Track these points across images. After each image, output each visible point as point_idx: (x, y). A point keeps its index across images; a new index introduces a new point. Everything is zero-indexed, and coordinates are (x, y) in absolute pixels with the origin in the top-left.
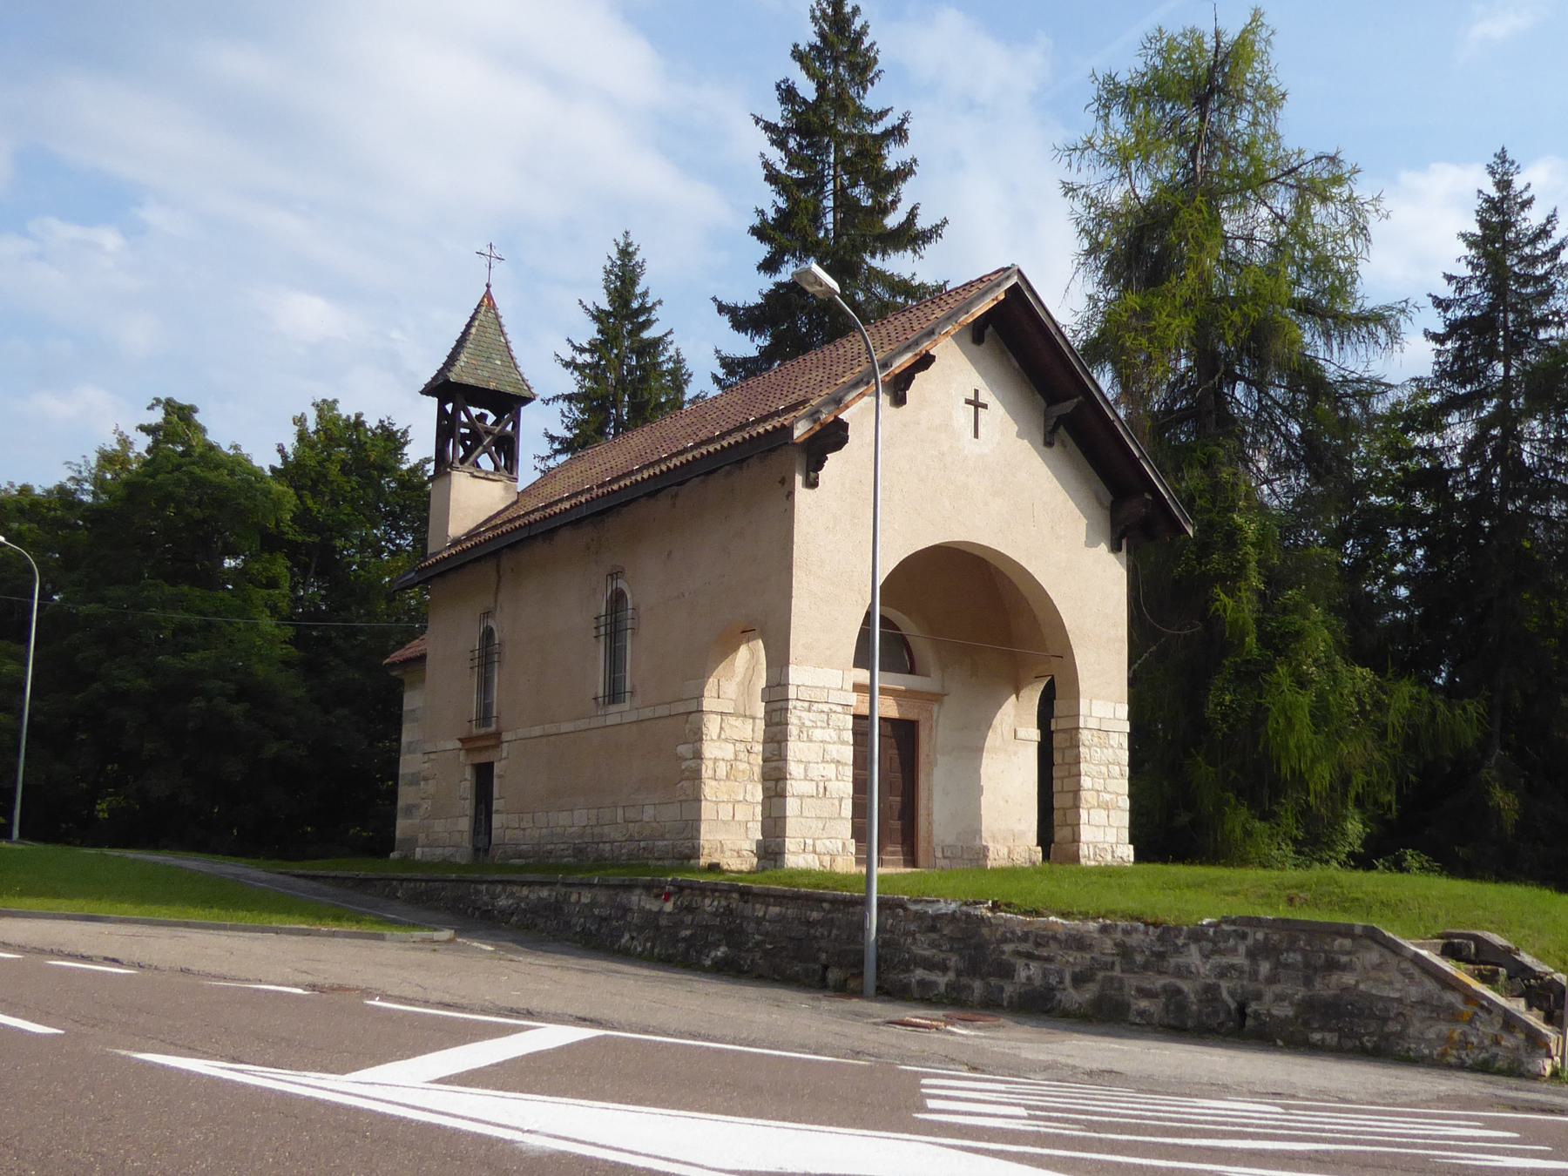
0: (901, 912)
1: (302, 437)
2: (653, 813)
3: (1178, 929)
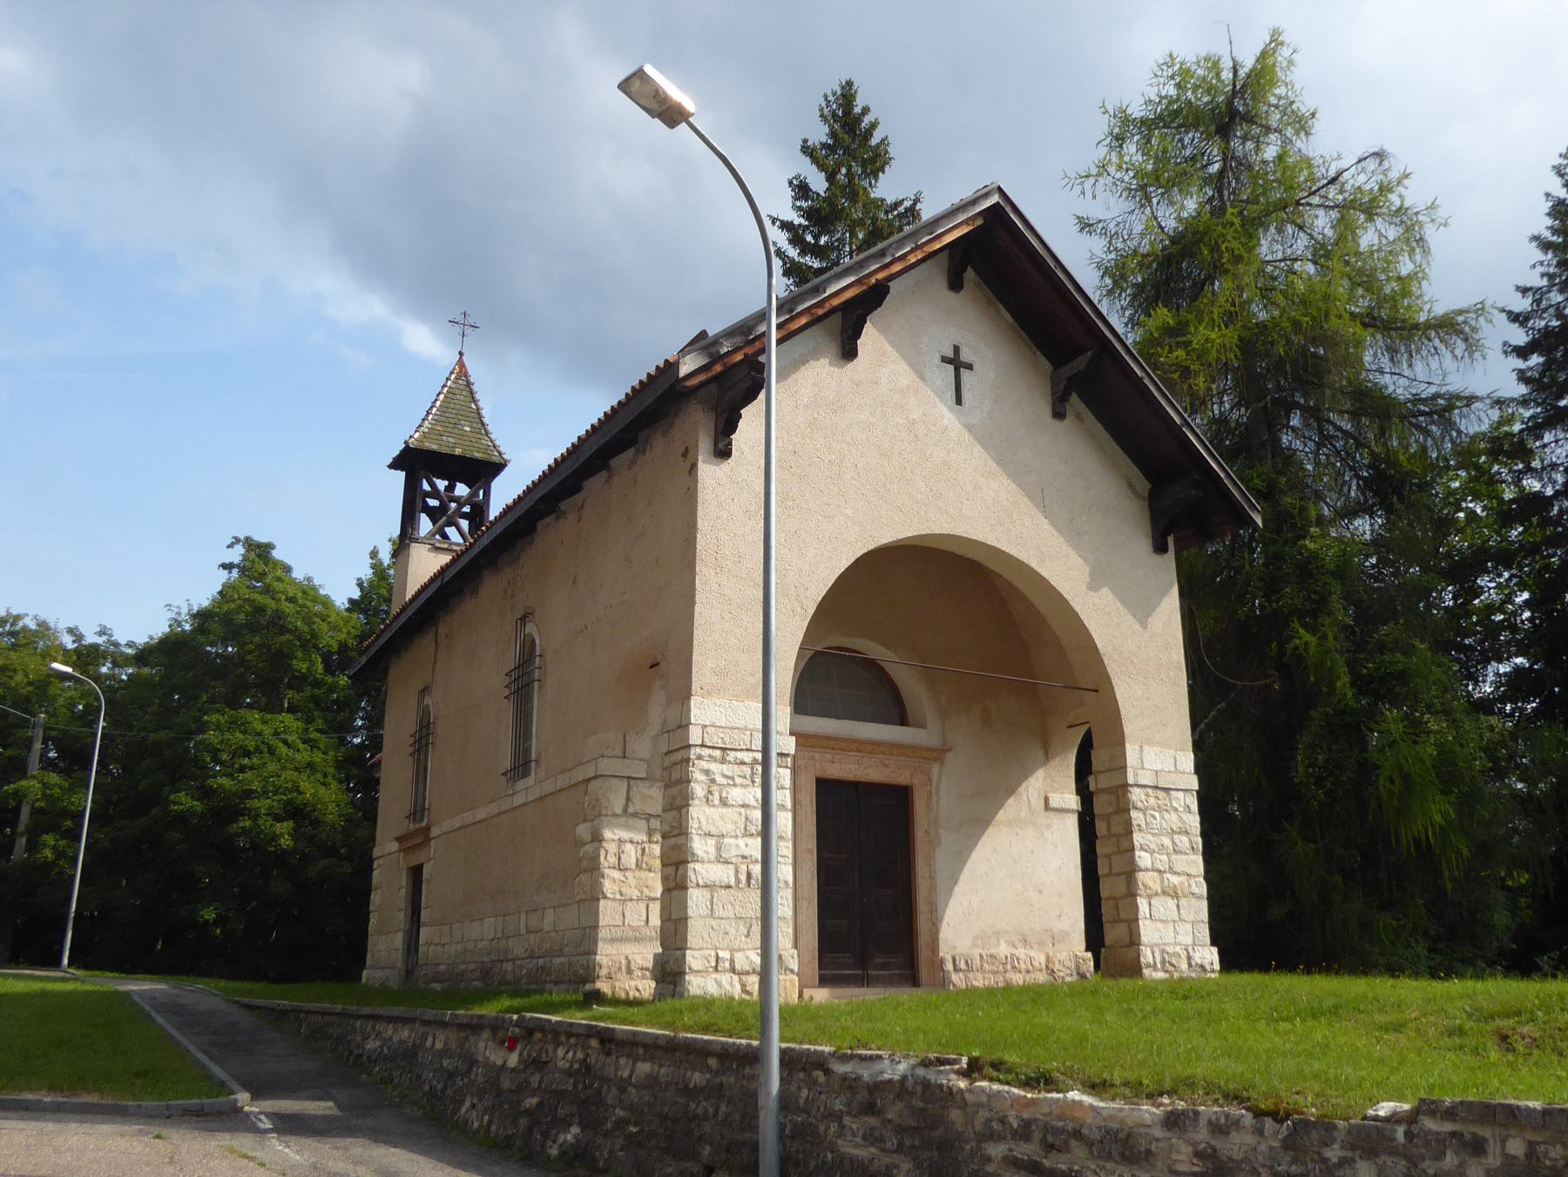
0: (820, 1076)
3: (1325, 1126)
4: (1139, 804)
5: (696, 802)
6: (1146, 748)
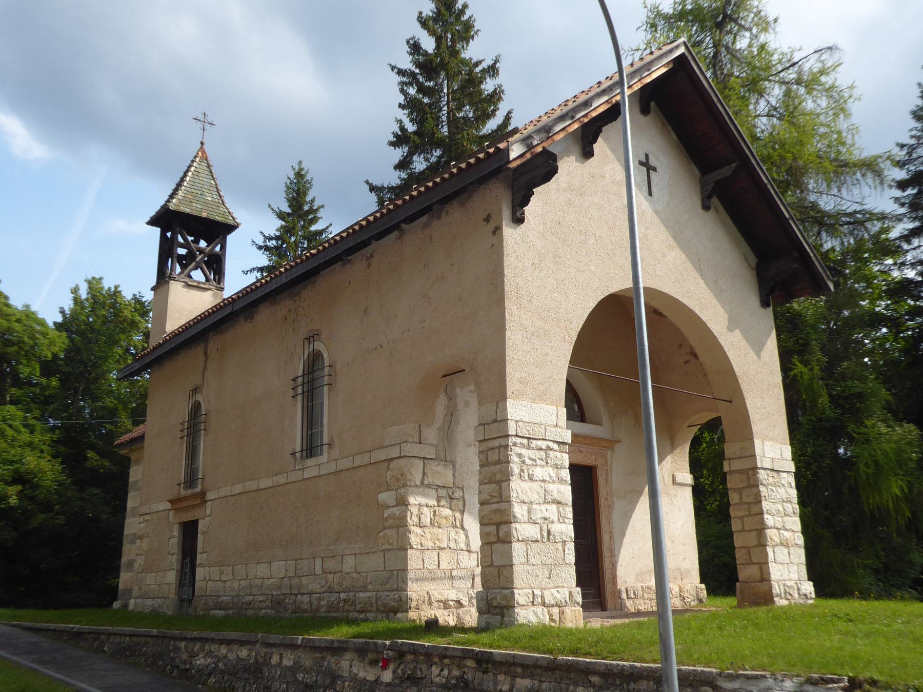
1: (77, 300)
2: (356, 564)
4: (764, 482)
5: (514, 478)
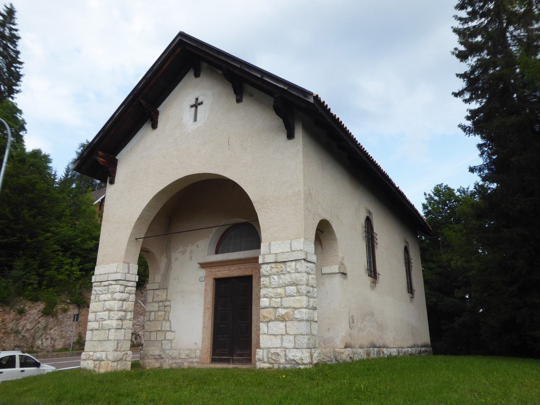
6: (272, 243)
